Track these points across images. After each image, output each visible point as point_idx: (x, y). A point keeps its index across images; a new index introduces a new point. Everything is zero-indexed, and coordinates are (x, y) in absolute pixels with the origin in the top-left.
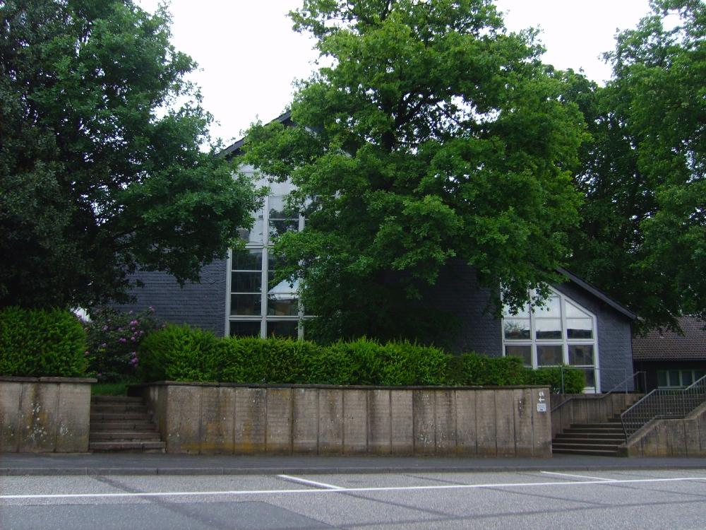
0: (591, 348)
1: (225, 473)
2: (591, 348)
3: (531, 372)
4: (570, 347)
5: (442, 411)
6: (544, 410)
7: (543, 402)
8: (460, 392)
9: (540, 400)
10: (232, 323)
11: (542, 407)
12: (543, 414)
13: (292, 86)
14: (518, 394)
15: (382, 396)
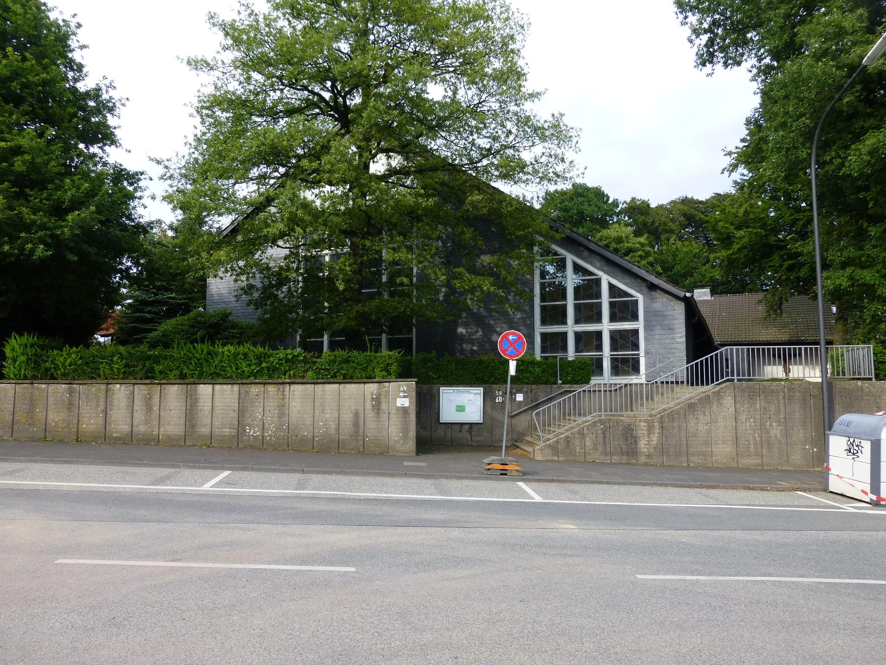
0: (544, 322)
1: (607, 483)
2: (544, 322)
3: (565, 362)
4: (577, 321)
5: (272, 405)
6: (407, 405)
7: (405, 397)
8: (296, 386)
9: (401, 394)
10: (544, 336)
11: (404, 402)
12: (404, 410)
13: (534, 113)
14: (371, 388)
15: (204, 390)
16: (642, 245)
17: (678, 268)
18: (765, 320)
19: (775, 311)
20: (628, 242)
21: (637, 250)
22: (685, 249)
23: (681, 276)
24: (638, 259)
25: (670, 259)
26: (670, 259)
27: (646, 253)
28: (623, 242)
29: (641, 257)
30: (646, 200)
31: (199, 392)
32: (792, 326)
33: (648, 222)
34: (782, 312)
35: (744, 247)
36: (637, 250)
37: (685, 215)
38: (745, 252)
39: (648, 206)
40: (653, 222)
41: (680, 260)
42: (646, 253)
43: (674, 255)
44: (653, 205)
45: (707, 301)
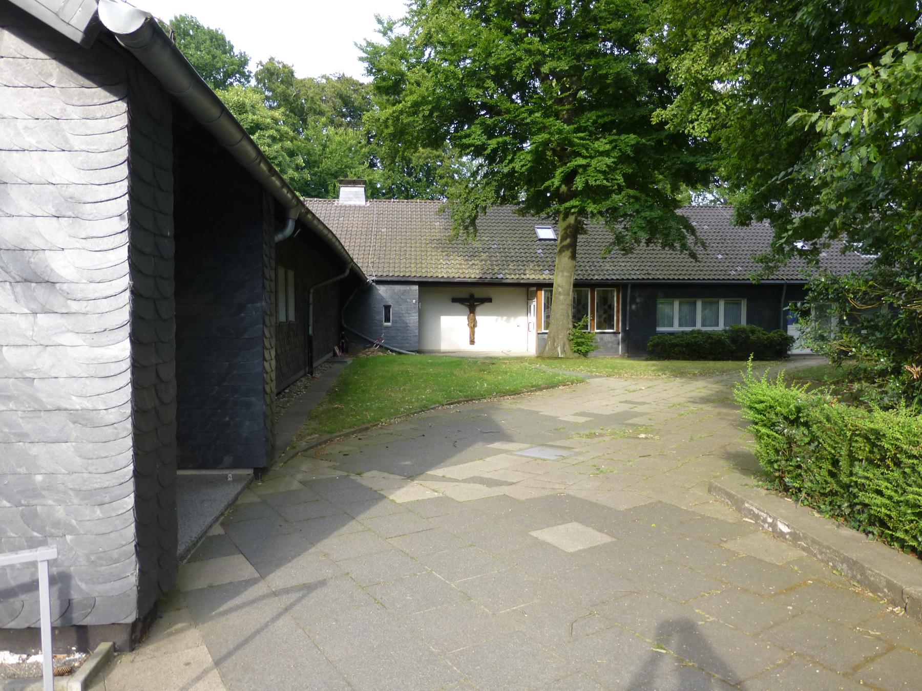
16: (276, 121)
17: (326, 164)
18: (448, 245)
19: (466, 228)
20: (254, 114)
21: (267, 128)
22: (338, 138)
23: (331, 174)
24: (269, 141)
25: (318, 148)
26: (318, 148)
27: (282, 136)
28: (246, 112)
29: (274, 139)
30: (290, 65)
31: (659, 313)
32: (484, 256)
33: (290, 96)
34: (476, 230)
35: (424, 101)
36: (267, 128)
37: (341, 96)
38: (426, 110)
39: (292, 73)
40: (297, 97)
41: (331, 153)
42: (282, 136)
43: (325, 147)
44: (299, 75)
45: (360, 207)
